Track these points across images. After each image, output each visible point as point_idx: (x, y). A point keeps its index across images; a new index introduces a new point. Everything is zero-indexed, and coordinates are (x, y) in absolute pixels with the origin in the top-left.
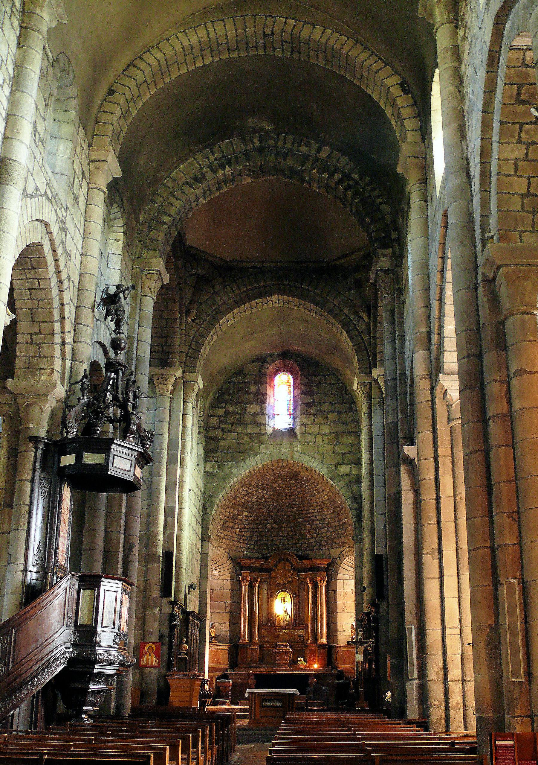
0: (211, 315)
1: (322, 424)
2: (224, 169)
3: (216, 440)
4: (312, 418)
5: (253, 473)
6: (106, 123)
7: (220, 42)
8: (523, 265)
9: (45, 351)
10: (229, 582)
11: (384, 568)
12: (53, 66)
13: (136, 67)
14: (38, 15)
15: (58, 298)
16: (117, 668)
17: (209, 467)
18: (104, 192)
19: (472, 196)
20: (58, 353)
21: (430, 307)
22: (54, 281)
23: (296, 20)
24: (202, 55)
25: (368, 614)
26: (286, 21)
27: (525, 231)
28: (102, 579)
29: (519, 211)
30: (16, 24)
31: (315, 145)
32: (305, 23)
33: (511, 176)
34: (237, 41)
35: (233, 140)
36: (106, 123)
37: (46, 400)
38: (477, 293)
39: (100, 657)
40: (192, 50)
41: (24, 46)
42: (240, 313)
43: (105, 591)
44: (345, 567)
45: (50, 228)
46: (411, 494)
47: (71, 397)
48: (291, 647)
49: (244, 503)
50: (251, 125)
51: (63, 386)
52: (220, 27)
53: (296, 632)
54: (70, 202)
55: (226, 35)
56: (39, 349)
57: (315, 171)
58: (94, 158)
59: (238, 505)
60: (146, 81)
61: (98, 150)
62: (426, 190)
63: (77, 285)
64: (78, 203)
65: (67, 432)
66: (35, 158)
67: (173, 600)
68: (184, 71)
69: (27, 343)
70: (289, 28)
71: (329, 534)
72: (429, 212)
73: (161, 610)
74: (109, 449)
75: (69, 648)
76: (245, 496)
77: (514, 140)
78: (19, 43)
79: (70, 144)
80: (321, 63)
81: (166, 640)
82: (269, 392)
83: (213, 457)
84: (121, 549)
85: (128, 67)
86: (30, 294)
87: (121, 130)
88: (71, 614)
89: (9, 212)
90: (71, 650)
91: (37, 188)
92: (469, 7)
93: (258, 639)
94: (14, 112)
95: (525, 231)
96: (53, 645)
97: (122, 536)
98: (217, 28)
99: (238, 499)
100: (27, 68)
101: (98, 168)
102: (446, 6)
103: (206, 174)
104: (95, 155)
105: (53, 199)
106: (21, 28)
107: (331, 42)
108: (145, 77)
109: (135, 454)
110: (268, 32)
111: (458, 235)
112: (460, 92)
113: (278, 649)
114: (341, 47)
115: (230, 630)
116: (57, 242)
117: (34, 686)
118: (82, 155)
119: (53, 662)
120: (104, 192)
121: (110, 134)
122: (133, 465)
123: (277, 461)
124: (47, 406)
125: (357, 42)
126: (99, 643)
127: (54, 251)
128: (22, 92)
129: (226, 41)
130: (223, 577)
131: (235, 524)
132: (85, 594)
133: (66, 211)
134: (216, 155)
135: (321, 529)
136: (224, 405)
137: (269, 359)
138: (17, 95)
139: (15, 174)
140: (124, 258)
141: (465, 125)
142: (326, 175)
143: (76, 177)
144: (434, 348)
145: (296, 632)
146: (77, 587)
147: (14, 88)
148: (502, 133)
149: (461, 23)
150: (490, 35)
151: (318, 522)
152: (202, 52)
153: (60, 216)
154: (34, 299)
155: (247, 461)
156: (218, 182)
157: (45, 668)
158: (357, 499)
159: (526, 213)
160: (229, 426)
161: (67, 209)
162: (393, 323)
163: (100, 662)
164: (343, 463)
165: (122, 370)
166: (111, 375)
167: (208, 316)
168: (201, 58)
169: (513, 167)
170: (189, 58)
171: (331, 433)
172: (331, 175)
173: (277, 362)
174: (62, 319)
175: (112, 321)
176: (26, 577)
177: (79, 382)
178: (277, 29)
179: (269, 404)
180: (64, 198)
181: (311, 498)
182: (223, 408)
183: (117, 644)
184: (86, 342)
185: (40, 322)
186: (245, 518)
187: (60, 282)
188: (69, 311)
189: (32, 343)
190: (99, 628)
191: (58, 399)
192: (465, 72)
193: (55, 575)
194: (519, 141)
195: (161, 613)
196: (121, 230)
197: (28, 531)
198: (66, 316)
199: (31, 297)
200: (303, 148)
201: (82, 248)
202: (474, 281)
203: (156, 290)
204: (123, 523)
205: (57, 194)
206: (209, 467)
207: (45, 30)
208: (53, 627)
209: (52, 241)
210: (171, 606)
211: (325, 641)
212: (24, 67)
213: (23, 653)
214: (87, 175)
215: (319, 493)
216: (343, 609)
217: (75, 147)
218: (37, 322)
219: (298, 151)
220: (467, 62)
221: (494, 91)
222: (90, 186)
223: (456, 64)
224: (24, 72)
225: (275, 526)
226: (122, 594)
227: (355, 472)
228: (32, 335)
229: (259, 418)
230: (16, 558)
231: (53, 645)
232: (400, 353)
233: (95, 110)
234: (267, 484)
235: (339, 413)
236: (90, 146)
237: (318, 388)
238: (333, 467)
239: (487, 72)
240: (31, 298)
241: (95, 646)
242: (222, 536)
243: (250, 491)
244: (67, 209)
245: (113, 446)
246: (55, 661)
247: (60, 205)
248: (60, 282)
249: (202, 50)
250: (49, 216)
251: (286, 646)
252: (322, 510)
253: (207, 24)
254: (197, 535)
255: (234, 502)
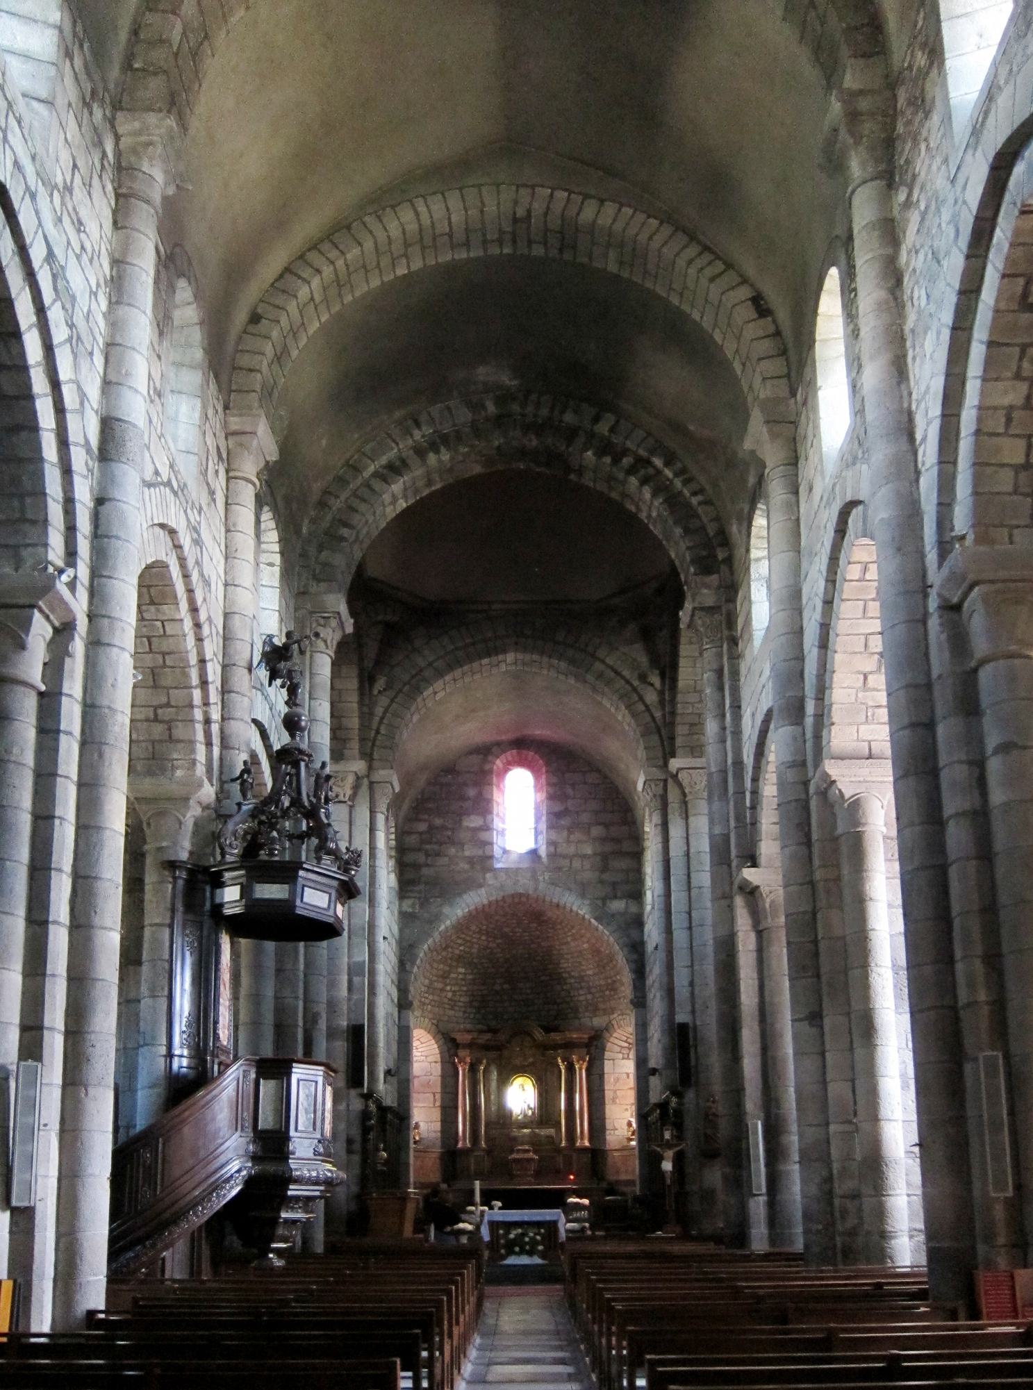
0: (408, 683)
1: (579, 842)
2: (437, 452)
3: (416, 866)
4: (565, 833)
5: (474, 913)
6: (251, 370)
7: (438, 232)
8: (1015, 581)
9: (179, 731)
10: (439, 1066)
11: (691, 1043)
12: (166, 267)
13: (296, 275)
14: (144, 173)
15: (195, 650)
16: (322, 1188)
17: (407, 906)
18: (254, 484)
19: (918, 473)
20: (200, 736)
21: (803, 660)
22: (188, 625)
23: (570, 192)
24: (406, 255)
25: (663, 1106)
26: (552, 194)
27: (1018, 527)
28: (294, 1065)
29: (1010, 494)
30: (109, 187)
31: (588, 411)
32: (586, 196)
33: (998, 435)
34: (466, 229)
35: (452, 403)
36: (251, 370)
37: (187, 807)
38: (926, 631)
39: (298, 1173)
40: (390, 244)
41: (125, 227)
42: (455, 680)
43: (299, 1081)
44: (616, 1041)
45: (178, 539)
46: (752, 937)
47: (224, 801)
48: (535, 1152)
49: (460, 956)
50: (481, 378)
51: (212, 785)
52: (437, 207)
53: (544, 1132)
54: (204, 499)
55: (449, 219)
56: (170, 729)
57: (589, 453)
58: (234, 427)
59: (451, 959)
60: (312, 299)
61: (241, 415)
62: (797, 475)
63: (221, 632)
64: (214, 500)
65: (223, 854)
66: (150, 422)
67: (365, 1091)
68: (375, 283)
69: (147, 720)
70: (557, 207)
71: (589, 997)
72: (802, 510)
73: (348, 1105)
74: (296, 877)
75: (247, 1161)
76: (461, 945)
77: (1009, 374)
78: (115, 223)
79: (198, 403)
80: (612, 267)
81: (357, 1146)
82: (496, 796)
83: (411, 891)
84: (301, 1023)
85: (281, 276)
86: (150, 644)
87: (275, 383)
88: (248, 1116)
89: (124, 506)
90: (250, 1164)
91: (157, 473)
92: (923, 147)
93: (485, 1142)
94: (119, 340)
95: (1018, 527)
96: (222, 1159)
97: (301, 1004)
98: (434, 208)
99: (450, 950)
100: (134, 265)
101: (241, 445)
102: (871, 149)
103: (408, 461)
104: (235, 423)
105: (180, 493)
106: (118, 196)
107: (631, 232)
108: (311, 293)
109: (335, 883)
110: (521, 212)
111: (893, 538)
112: (896, 299)
113: (515, 1156)
114: (650, 238)
115: (442, 1131)
116: (190, 563)
117: (197, 1217)
118: (216, 421)
119: (224, 1182)
120: (254, 484)
121: (258, 387)
122: (333, 898)
123: (513, 896)
124: (189, 815)
125: (677, 230)
126: (293, 1153)
127: (186, 576)
128: (129, 305)
129: (447, 230)
130: (430, 1059)
131: (446, 985)
132: (267, 1087)
133: (200, 513)
134: (424, 428)
135: (578, 989)
136: (426, 817)
137: (495, 749)
138: (122, 311)
139: (129, 444)
140: (282, 592)
141: (905, 356)
142: (608, 460)
143: (210, 458)
144: (809, 721)
145: (544, 1132)
146: (253, 1076)
147: (114, 300)
148: (989, 363)
149: (901, 178)
150: (980, 190)
151: (573, 981)
152: (406, 250)
153: (192, 520)
154: (156, 653)
155: (465, 897)
156: (429, 474)
157: (213, 1191)
158: (637, 949)
159: (1021, 498)
160: (436, 847)
161: (200, 510)
162: (721, 688)
163: (297, 1181)
164: (615, 897)
165: (304, 761)
166: (286, 769)
167: (405, 684)
168: (404, 261)
169: (1003, 420)
170: (385, 261)
171: (595, 854)
172: (616, 461)
173: (508, 753)
174: (204, 683)
175: (282, 686)
176: (171, 1062)
177: (237, 779)
178: (538, 207)
179: (498, 815)
180: (196, 492)
181: (564, 947)
182: (425, 821)
183: (320, 1154)
184: (242, 720)
185: (168, 688)
186: (461, 976)
187: (198, 626)
188: (214, 672)
189: (156, 719)
190: (292, 1133)
191: (204, 805)
192: (908, 263)
193: (216, 1061)
194: (1018, 376)
195: (348, 1110)
196: (276, 548)
197: (170, 998)
198: (210, 679)
199: (150, 649)
200: (569, 417)
201: (226, 573)
202: (922, 610)
203: (335, 643)
204: (301, 985)
205: (185, 485)
206: (407, 906)
207: (157, 198)
208: (221, 1134)
209: (182, 561)
210: (363, 1100)
211: (587, 1144)
212: (128, 263)
213: (177, 1172)
214: (225, 456)
215: (574, 940)
216: (614, 1100)
217: (204, 407)
218: (164, 687)
219: (561, 421)
220: (914, 246)
221: (978, 290)
222: (231, 474)
223: (890, 251)
224: (129, 271)
225: (506, 986)
226: (324, 1085)
227: (633, 909)
228: (156, 708)
229: (483, 836)
230: (154, 1038)
231: (222, 1159)
232: (733, 733)
233: (230, 347)
234: (494, 929)
235: (606, 826)
236: (226, 407)
237: (574, 789)
238: (599, 903)
239: (968, 257)
240: (151, 651)
241: (288, 1158)
242: (427, 1001)
243: (468, 938)
244: (200, 510)
245: (301, 873)
246: (228, 1180)
247: (190, 503)
248: (198, 626)
249: (407, 245)
250: (177, 520)
251: (527, 1151)
252: (580, 963)
253: (414, 200)
254: (392, 1001)
255: (444, 953)
